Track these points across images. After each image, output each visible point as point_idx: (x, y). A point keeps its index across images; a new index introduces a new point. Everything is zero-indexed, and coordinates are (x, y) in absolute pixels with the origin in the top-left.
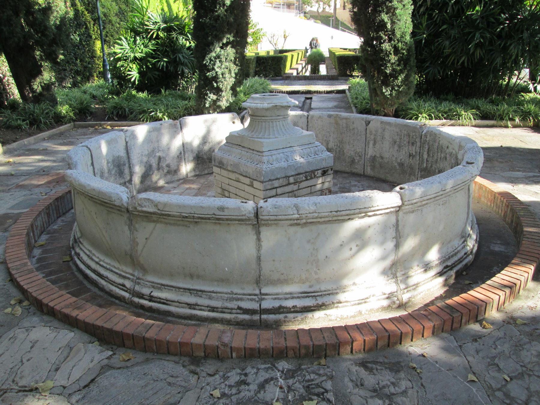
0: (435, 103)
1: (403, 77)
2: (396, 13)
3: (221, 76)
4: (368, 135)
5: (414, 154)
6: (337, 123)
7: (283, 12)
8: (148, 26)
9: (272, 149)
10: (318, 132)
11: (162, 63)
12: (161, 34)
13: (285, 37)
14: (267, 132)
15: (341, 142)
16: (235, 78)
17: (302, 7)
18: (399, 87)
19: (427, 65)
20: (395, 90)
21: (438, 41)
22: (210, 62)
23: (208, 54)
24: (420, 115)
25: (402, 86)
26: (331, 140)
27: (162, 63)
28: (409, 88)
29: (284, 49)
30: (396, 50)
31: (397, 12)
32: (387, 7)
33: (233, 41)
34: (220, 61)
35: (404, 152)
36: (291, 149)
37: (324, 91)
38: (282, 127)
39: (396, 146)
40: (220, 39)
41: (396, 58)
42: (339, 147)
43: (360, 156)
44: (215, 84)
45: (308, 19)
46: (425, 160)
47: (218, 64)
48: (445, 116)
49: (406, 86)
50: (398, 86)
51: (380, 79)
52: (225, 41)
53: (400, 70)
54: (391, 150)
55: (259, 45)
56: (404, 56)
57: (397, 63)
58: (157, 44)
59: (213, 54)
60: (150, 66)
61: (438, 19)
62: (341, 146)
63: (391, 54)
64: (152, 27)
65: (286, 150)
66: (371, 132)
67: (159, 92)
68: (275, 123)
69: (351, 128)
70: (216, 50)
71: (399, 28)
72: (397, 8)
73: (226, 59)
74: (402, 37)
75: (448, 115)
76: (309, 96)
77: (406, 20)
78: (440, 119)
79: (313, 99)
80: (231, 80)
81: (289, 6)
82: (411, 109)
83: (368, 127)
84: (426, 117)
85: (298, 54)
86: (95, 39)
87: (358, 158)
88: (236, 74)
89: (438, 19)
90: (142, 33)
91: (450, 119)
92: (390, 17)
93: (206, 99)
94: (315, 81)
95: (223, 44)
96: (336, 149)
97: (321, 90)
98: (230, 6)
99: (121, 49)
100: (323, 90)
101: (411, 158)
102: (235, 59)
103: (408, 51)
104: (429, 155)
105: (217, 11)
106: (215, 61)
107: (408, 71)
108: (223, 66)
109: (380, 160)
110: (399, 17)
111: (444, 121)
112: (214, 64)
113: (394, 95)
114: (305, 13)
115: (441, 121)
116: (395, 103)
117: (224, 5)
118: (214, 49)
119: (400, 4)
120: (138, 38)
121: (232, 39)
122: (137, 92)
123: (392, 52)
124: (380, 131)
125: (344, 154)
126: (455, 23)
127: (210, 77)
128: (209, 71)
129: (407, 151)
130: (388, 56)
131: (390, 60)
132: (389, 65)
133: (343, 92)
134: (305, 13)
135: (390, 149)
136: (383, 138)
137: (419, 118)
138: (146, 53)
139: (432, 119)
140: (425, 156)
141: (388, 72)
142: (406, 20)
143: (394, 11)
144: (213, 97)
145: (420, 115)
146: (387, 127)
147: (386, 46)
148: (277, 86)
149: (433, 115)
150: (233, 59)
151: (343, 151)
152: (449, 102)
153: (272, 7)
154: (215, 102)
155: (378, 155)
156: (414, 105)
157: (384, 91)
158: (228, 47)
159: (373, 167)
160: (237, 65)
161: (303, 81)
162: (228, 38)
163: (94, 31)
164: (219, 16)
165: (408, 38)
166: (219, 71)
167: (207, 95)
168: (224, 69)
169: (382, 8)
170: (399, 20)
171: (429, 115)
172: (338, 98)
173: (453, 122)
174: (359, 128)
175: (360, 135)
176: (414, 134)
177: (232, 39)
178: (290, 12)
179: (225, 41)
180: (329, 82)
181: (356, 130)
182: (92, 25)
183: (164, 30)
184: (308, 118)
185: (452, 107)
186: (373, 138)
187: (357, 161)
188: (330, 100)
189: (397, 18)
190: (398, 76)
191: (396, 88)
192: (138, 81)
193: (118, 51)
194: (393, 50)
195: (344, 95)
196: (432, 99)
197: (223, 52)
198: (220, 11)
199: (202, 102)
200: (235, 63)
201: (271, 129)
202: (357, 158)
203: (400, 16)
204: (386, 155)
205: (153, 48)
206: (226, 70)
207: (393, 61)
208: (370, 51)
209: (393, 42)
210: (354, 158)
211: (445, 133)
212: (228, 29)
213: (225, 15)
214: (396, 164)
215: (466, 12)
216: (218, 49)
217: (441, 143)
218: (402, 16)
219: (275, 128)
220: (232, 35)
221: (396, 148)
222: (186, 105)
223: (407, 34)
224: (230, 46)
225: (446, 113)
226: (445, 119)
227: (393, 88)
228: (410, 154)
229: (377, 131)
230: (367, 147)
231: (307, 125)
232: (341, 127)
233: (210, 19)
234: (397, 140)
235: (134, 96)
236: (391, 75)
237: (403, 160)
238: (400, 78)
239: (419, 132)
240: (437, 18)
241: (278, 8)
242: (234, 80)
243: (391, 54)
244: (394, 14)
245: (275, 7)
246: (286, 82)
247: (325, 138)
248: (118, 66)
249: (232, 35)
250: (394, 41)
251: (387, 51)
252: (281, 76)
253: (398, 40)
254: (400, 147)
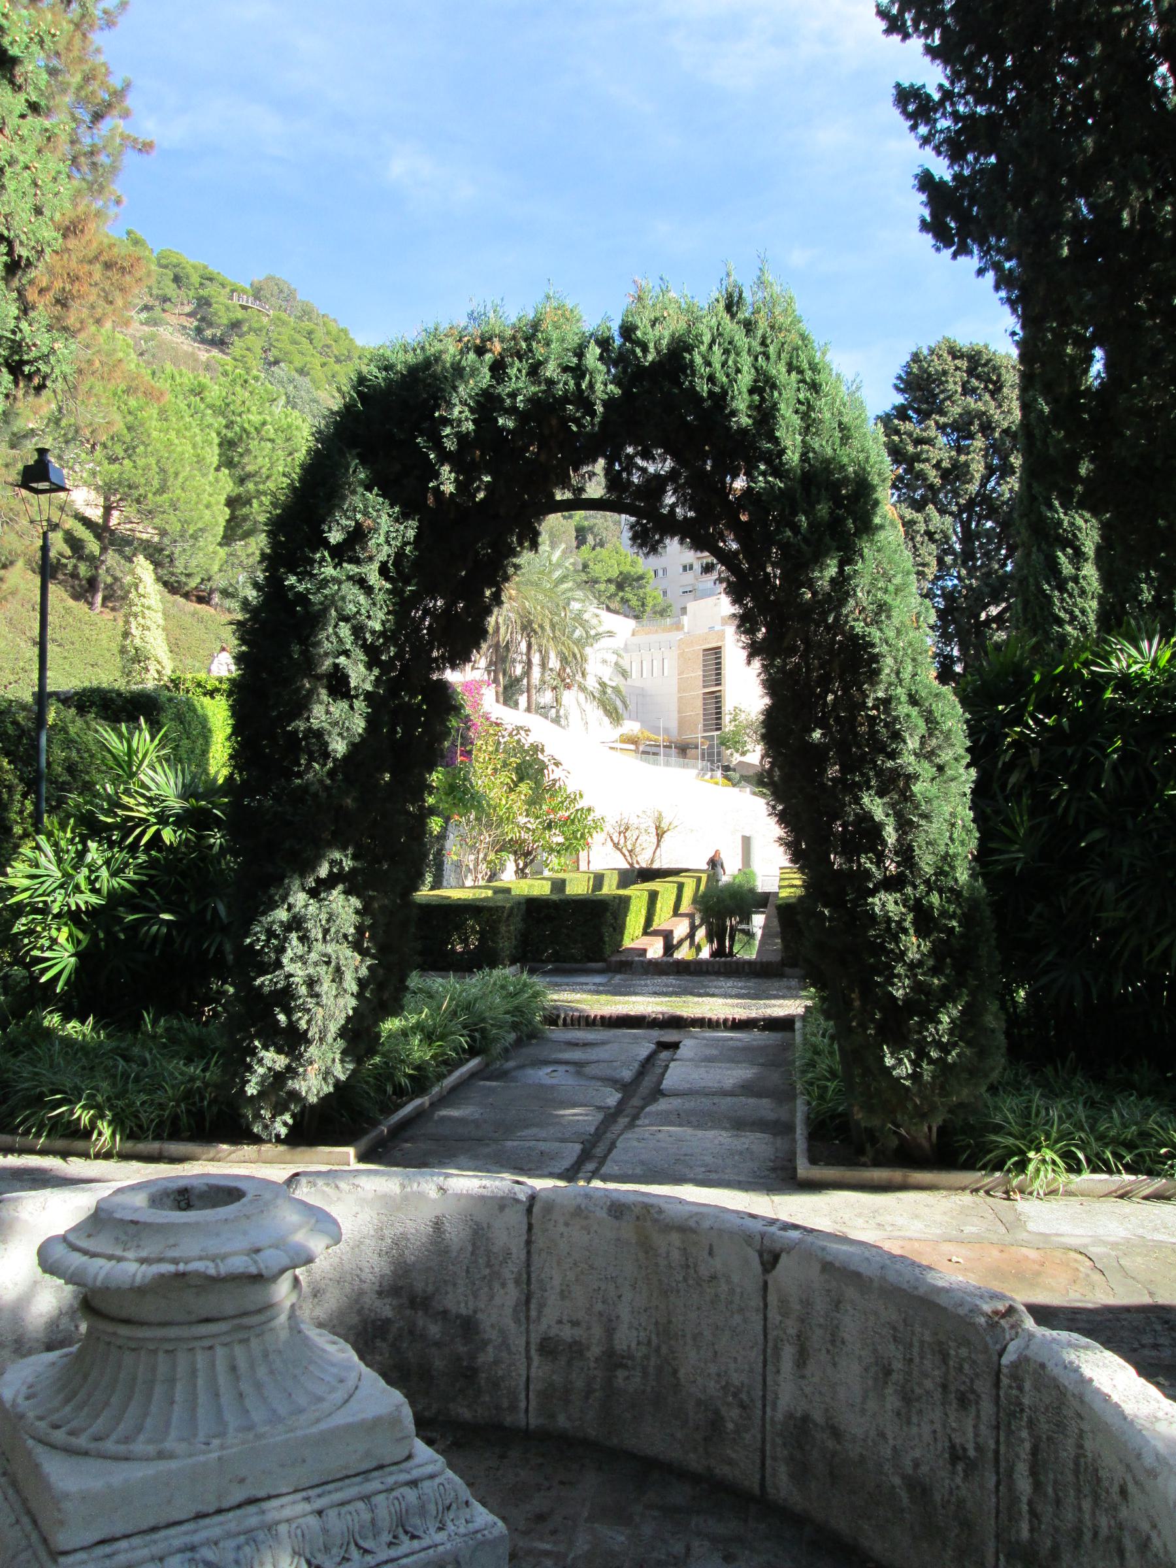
0: (1090, 1104)
1: (955, 1013)
2: (913, 795)
3: (303, 990)
4: (774, 1315)
5: (972, 1453)
6: (646, 1246)
7: (667, 764)
8: (131, 810)
9: (118, 1530)
10: (571, 1276)
11: (155, 928)
12: (168, 835)
13: (660, 836)
14: (133, 1409)
15: (665, 1331)
16: (359, 996)
17: (719, 754)
18: (945, 1049)
19: (1049, 958)
20: (931, 1061)
21: (1078, 881)
22: (268, 941)
23: (264, 913)
24: (1031, 1154)
25: (955, 1045)
26: (624, 1312)
27: (155, 928)
28: (982, 1053)
29: (656, 866)
30: (924, 920)
31: (917, 788)
32: (880, 772)
33: (353, 870)
34: (300, 939)
35: (926, 1430)
36: (251, 1518)
37: (726, 1020)
38: (223, 1379)
39: (890, 1390)
40: (306, 866)
41: (926, 946)
42: (658, 1350)
43: (743, 1406)
44: (282, 1017)
45: (734, 785)
46: (1025, 1508)
47: (294, 945)
48: (1128, 1159)
49: (969, 1043)
50: (939, 1045)
51: (873, 1020)
52: (323, 871)
53: (943, 987)
54: (872, 1405)
55: (583, 855)
56: (953, 941)
57: (931, 962)
58: (152, 863)
59: (282, 915)
60: (122, 937)
61: (1072, 812)
62: (664, 1350)
63: (905, 931)
64: (143, 811)
65: (212, 1528)
66: (783, 1302)
67: (136, 1024)
68: (182, 1359)
69: (704, 1272)
70: (291, 900)
71: (928, 843)
72: (916, 777)
73: (326, 932)
74: (940, 872)
75: (1140, 1155)
76: (670, 1036)
77: (953, 815)
78: (1110, 1171)
79: (683, 1052)
80: (341, 1002)
81: (684, 749)
82: (998, 1129)
83: (770, 1278)
84: (1054, 1162)
85: (681, 887)
86: (21, 838)
87: (735, 1413)
88: (361, 982)
89: (1072, 812)
90: (109, 827)
91: (1150, 1173)
92: (893, 805)
93: (249, 1069)
94: (705, 980)
95: (318, 881)
96: (646, 1357)
97: (714, 1017)
98: (345, 757)
99: (32, 877)
100: (722, 1017)
101: (960, 1468)
102: (360, 929)
103: (967, 920)
104: (1037, 1486)
105: (299, 775)
106: (286, 939)
107: (972, 994)
108: (313, 956)
109: (830, 1444)
110: (924, 807)
111: (1128, 1178)
112: (281, 950)
113: (927, 1077)
114: (726, 768)
115: (1116, 1177)
116: (933, 1108)
117: (326, 754)
118: (284, 898)
119: (926, 765)
120: (92, 845)
121: (348, 864)
122: (66, 1019)
123: (907, 924)
124: (820, 1305)
125: (677, 1386)
126: (1130, 824)
127: (266, 990)
128: (264, 970)
129: (938, 1426)
130: (897, 940)
131: (903, 953)
132: (900, 969)
133: (784, 1024)
134: (726, 768)
135: (865, 1398)
136: (834, 1338)
137: (1031, 1167)
138: (112, 894)
139: (1079, 1171)
140: (1024, 1485)
141: (899, 994)
142: (953, 815)
143: (907, 786)
144: (273, 1059)
145: (1031, 1154)
146: (851, 1293)
147: (887, 904)
148: (578, 996)
149: (1081, 1156)
150: (352, 930)
151: (675, 1372)
152: (1141, 1097)
153: (636, 751)
154: (278, 1078)
155: (818, 1416)
156: (1007, 1110)
157: (889, 1061)
158: (335, 892)
159: (801, 1472)
160: (364, 953)
161: (671, 980)
162: (333, 863)
163: (21, 812)
164: (305, 788)
165: (962, 875)
166: (298, 972)
167: (253, 1052)
168: (316, 964)
169: (862, 775)
170: (926, 816)
171: (1067, 1156)
172: (762, 1049)
173: (1159, 1183)
174: (736, 1279)
175: (741, 1310)
176: (964, 1352)
177: (348, 864)
178: (684, 766)
179: (323, 871)
180: (751, 983)
181: (724, 1287)
182: (18, 797)
183: (180, 821)
184: (529, 1211)
185: (1151, 1124)
186: (792, 1331)
187: (730, 1426)
188: (734, 1055)
189: (917, 807)
190: (937, 1011)
191: (934, 1054)
192: (67, 983)
193: (20, 882)
194: (910, 917)
195: (788, 1035)
196: (1078, 1081)
197: (312, 909)
198: (310, 775)
199: (235, 1075)
200: (357, 946)
201: (159, 1390)
202: (732, 1414)
203: (928, 801)
204: (856, 1426)
205: (136, 877)
206: (322, 969)
207: (912, 955)
208: (830, 919)
209: (909, 890)
210: (717, 1412)
211: (1106, 1398)
212: (334, 834)
213: (327, 788)
214: (897, 1481)
215: (1163, 791)
216: (299, 898)
217: (1088, 1444)
218: (935, 803)
219: (179, 1387)
220: (350, 851)
221: (892, 1402)
222: (192, 1079)
223: (957, 863)
224: (340, 887)
225: (1130, 1146)
226: (1130, 1169)
227: (922, 1054)
228: (953, 1447)
229: (807, 1303)
230: (770, 1367)
231: (529, 1243)
232: (663, 1262)
233: (276, 798)
234: (897, 1365)
235: (49, 1033)
236: (910, 1006)
237: (924, 1469)
238: (945, 1019)
239: (986, 1350)
240: (1067, 808)
241: (654, 754)
242: (353, 1002)
243: (905, 931)
244: (906, 796)
245: (644, 753)
246: (618, 979)
247: (599, 1307)
248: (15, 930)
249: (350, 851)
250: (915, 887)
251: (889, 920)
252: (604, 960)
253: (927, 882)
254: (907, 1398)
